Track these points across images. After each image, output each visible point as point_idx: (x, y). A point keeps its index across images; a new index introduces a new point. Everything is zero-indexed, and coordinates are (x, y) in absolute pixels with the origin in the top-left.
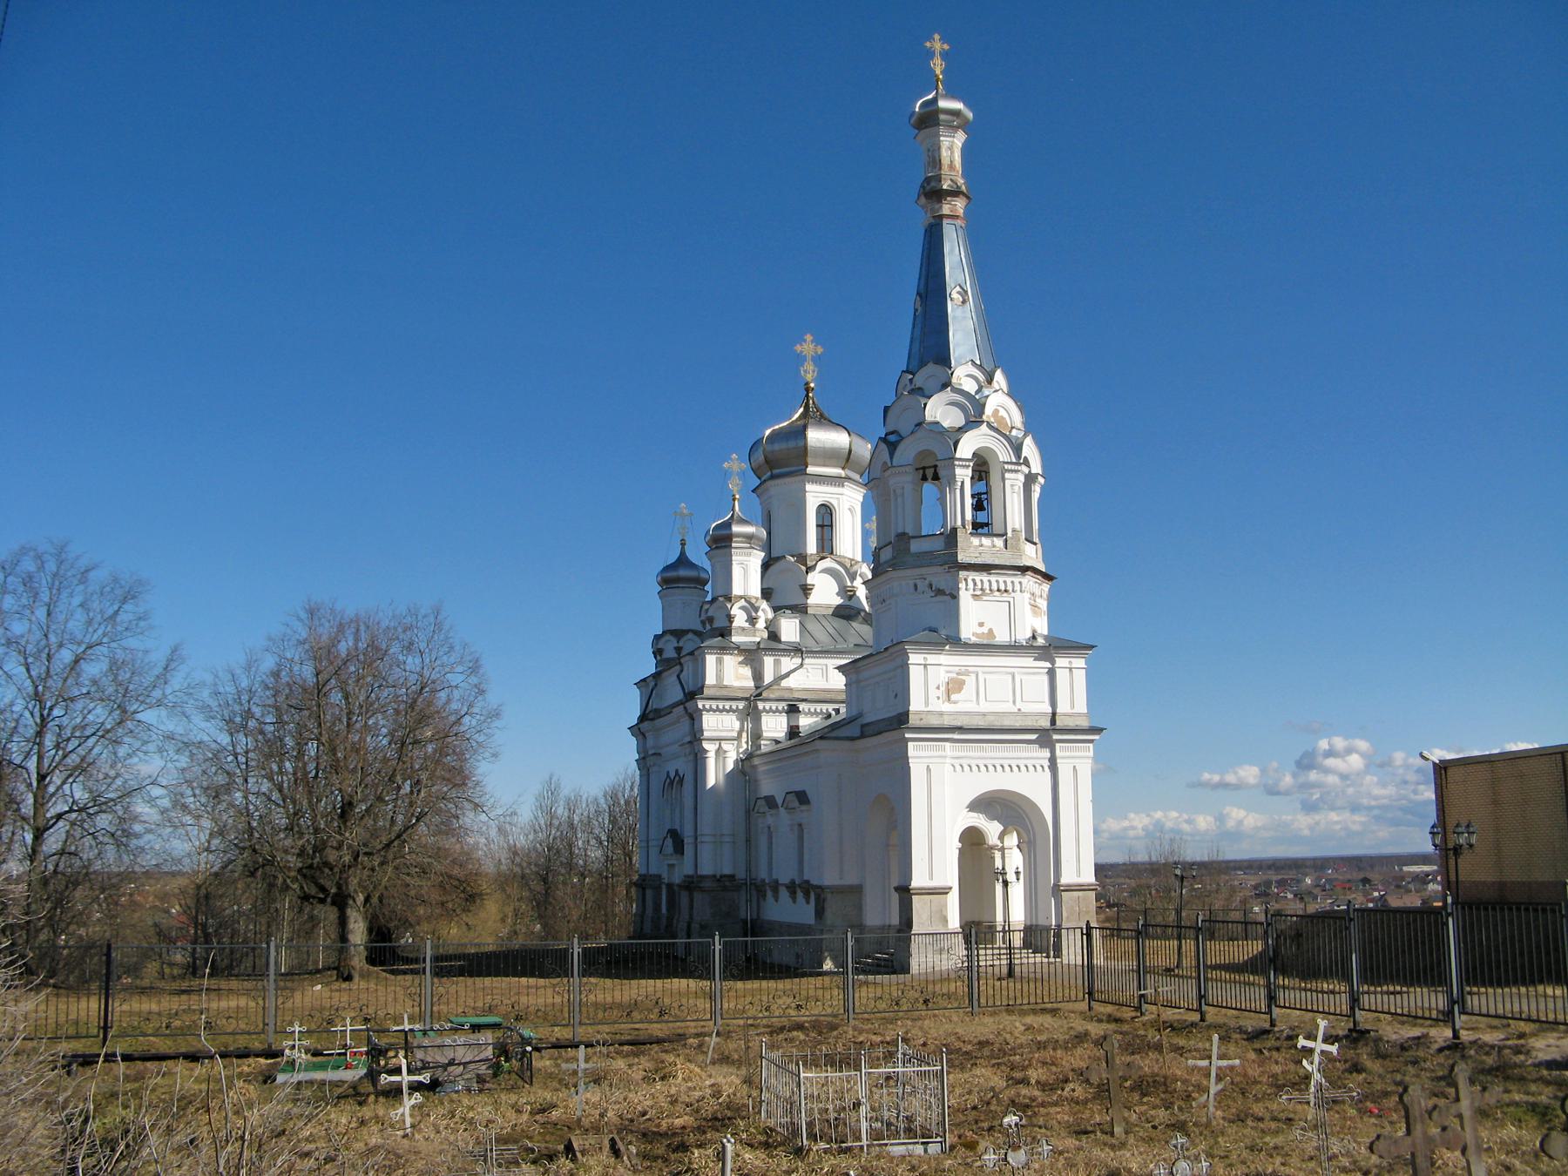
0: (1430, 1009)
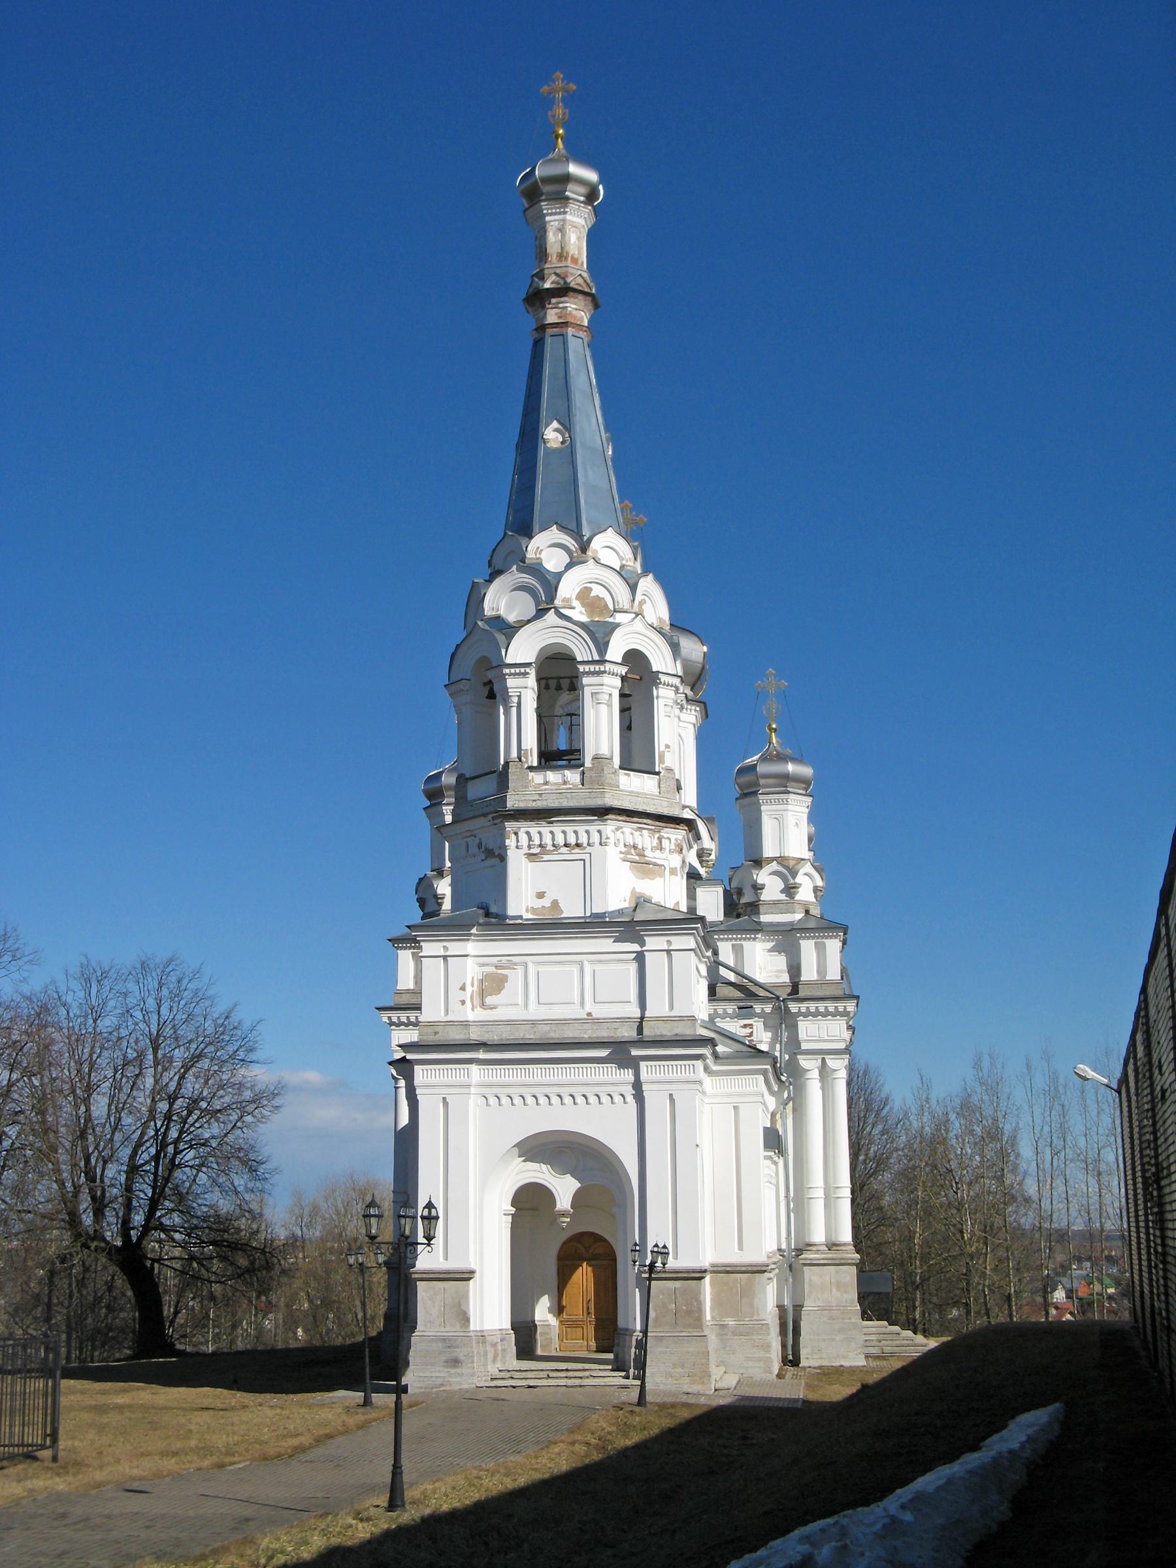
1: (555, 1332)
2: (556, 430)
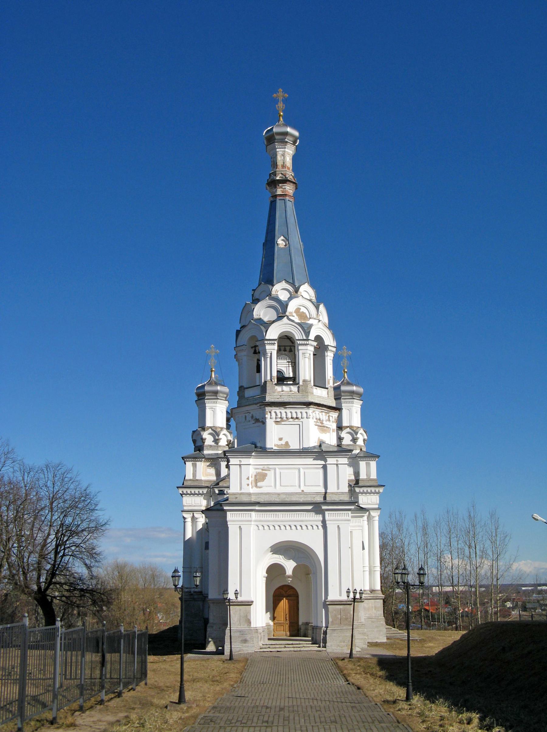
0: (11, 683)
1: (272, 628)
2: (283, 240)
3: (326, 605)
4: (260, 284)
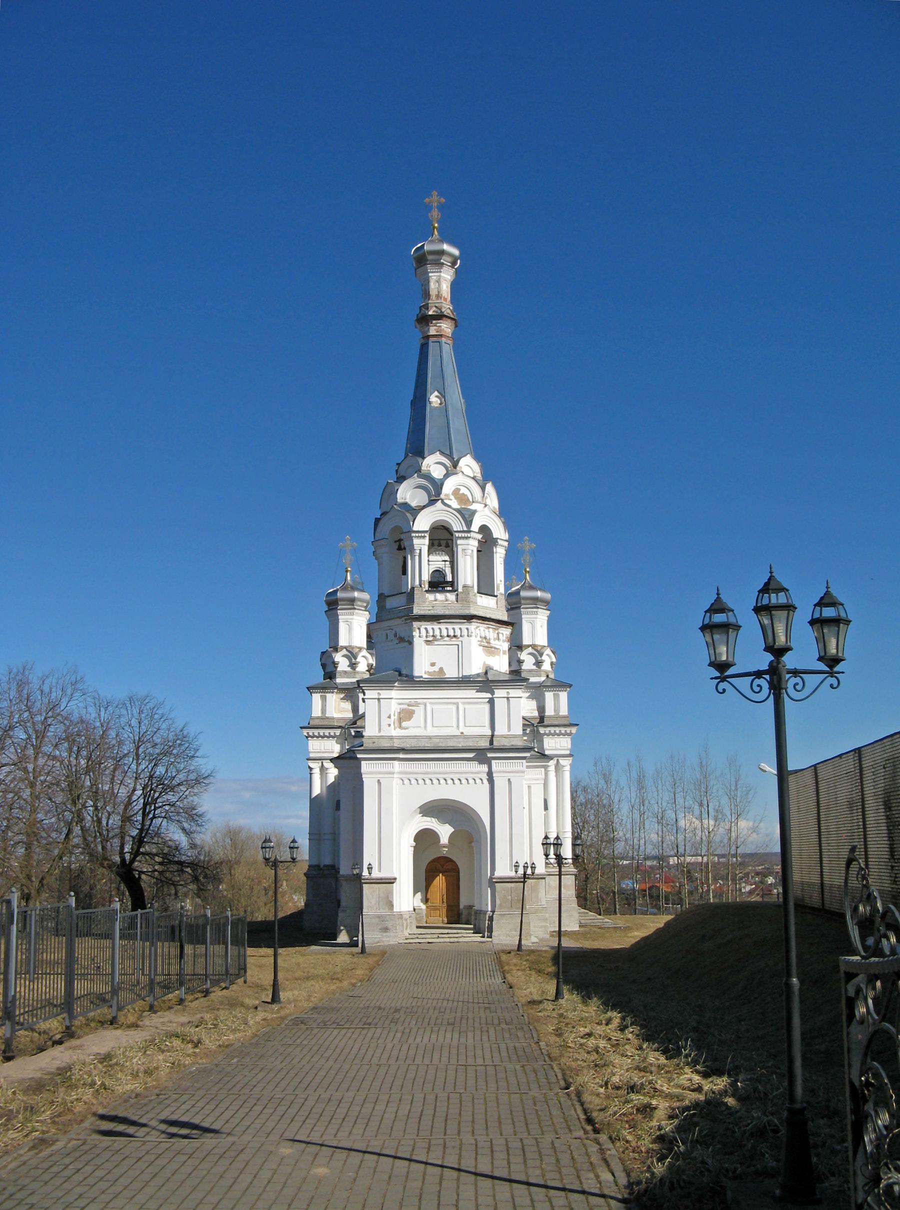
1: (424, 912)
2: (437, 397)
3: (493, 883)
4: (406, 456)
